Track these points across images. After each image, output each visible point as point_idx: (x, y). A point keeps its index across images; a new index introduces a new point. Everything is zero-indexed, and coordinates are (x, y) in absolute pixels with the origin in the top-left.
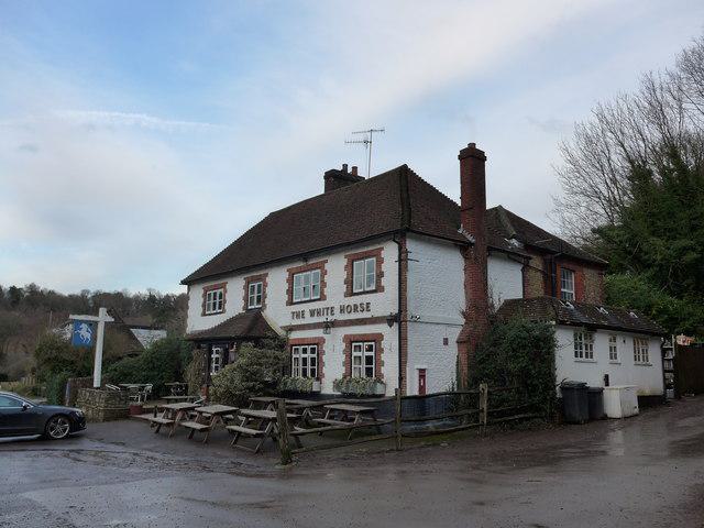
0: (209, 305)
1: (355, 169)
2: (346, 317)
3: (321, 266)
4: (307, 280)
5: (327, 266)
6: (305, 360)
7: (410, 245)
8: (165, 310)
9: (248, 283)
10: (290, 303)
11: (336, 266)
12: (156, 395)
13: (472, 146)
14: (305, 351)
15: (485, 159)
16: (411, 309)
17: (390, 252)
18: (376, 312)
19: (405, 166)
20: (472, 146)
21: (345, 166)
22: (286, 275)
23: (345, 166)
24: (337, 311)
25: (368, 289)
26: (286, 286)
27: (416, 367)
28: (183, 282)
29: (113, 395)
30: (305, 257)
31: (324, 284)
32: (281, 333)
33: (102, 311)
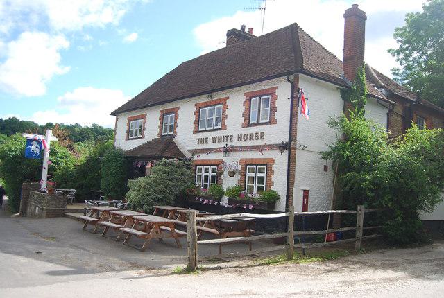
0: (132, 131)
1: (251, 29)
2: (243, 143)
3: (223, 102)
4: (211, 113)
5: (228, 102)
6: (206, 177)
7: (305, 86)
8: (98, 134)
9: (163, 115)
10: (197, 131)
11: (236, 103)
12: (79, 199)
13: (355, 6)
14: (206, 170)
15: (365, 18)
16: (300, 138)
17: (283, 92)
18: (269, 140)
19: (296, 24)
20: (355, 6)
21: (243, 27)
22: (159, 115)
23: (243, 27)
24: (235, 139)
25: (217, 127)
26: (194, 118)
27: (302, 188)
28: (113, 114)
29: (56, 198)
30: (210, 92)
31: (225, 117)
32: (189, 155)
33: (50, 132)
